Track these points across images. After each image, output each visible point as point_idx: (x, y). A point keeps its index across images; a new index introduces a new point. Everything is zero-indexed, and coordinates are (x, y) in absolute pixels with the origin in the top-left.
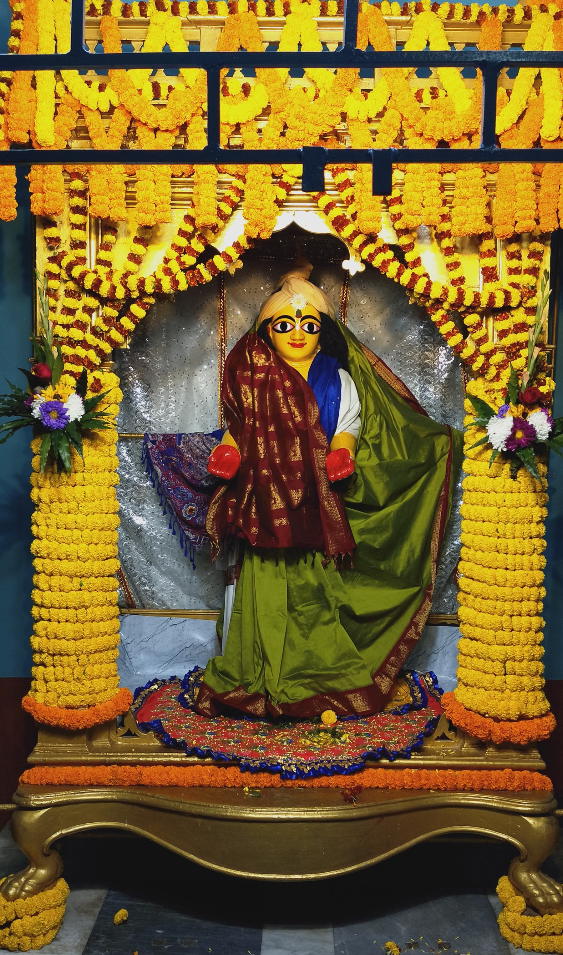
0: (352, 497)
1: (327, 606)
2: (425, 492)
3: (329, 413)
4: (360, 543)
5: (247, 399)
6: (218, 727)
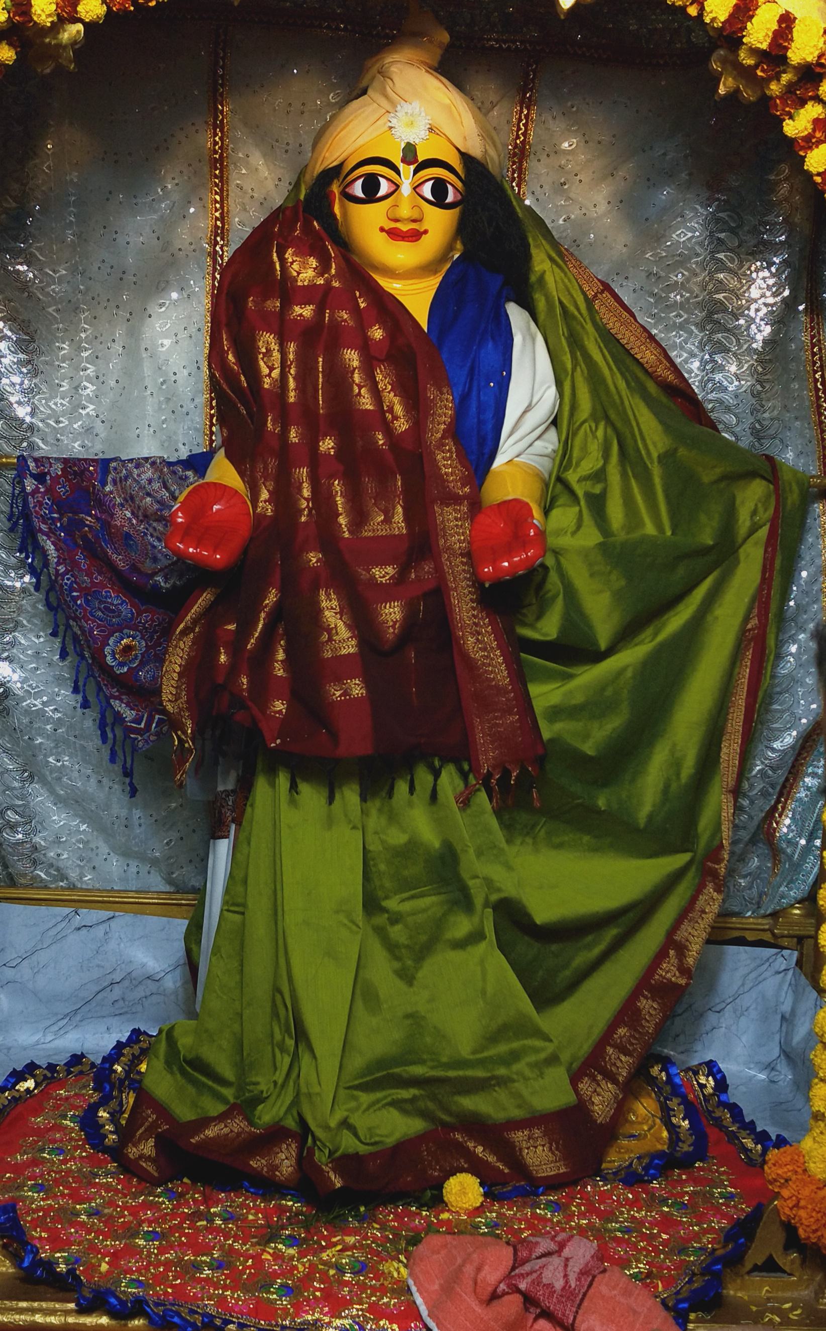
0: (532, 626)
1: (463, 900)
2: (709, 618)
3: (481, 409)
4: (551, 741)
5: (271, 369)
6: (173, 1216)
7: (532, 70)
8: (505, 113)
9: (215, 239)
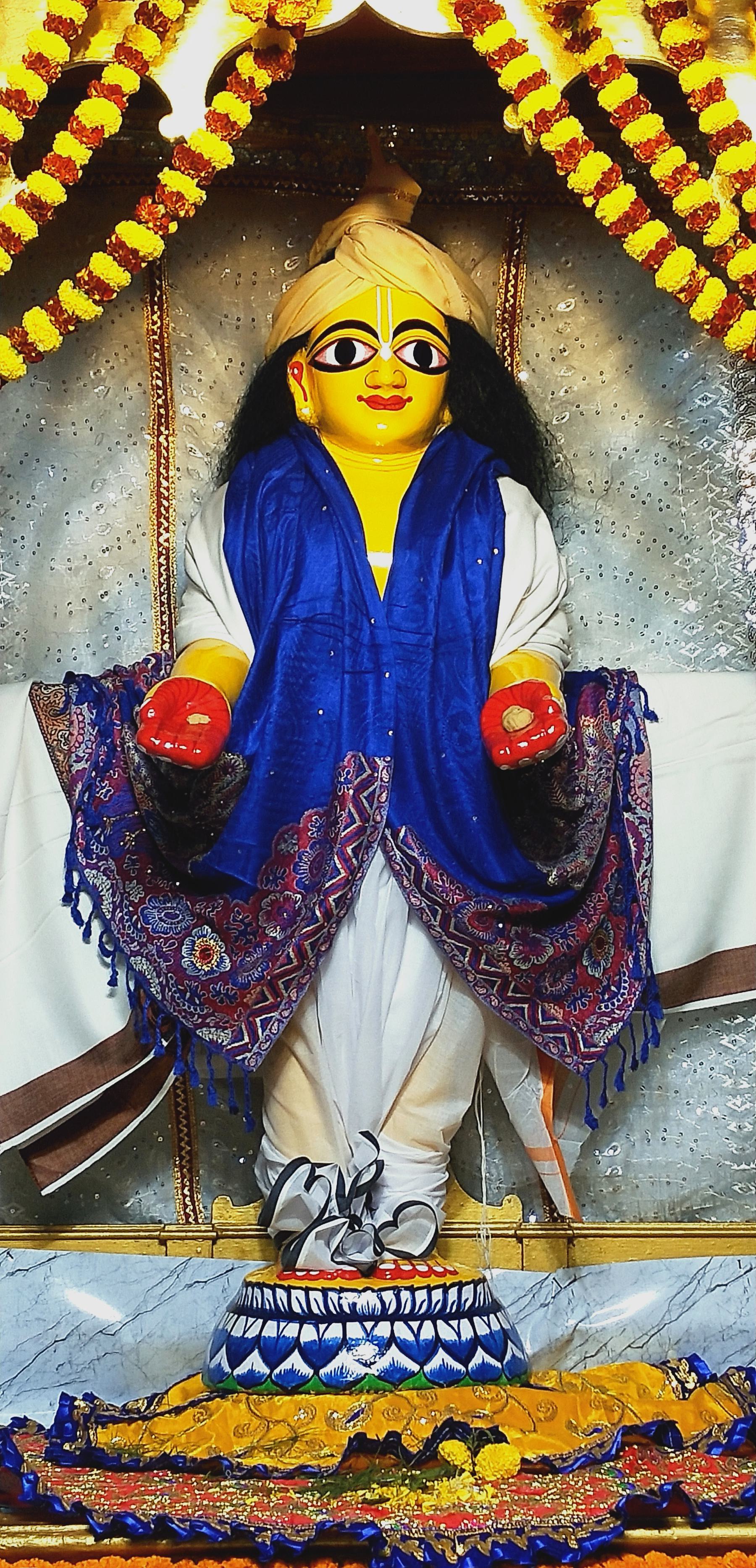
7: (518, 225)
8: (488, 274)
9: (159, 430)
